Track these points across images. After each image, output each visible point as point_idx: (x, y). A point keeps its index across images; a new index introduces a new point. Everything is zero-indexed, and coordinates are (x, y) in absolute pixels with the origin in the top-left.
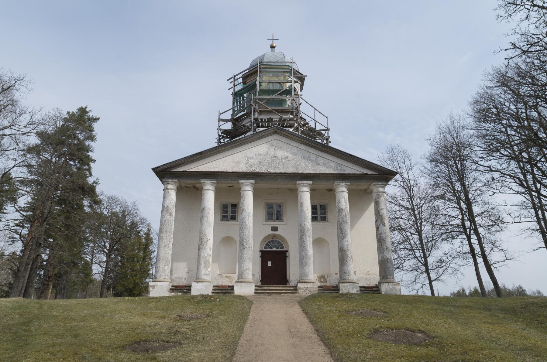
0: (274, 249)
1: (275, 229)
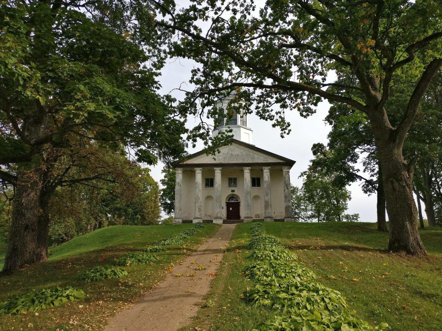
0: (233, 201)
1: (233, 191)
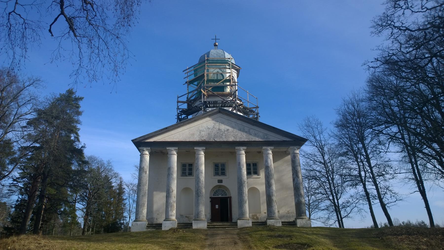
1: (220, 181)
